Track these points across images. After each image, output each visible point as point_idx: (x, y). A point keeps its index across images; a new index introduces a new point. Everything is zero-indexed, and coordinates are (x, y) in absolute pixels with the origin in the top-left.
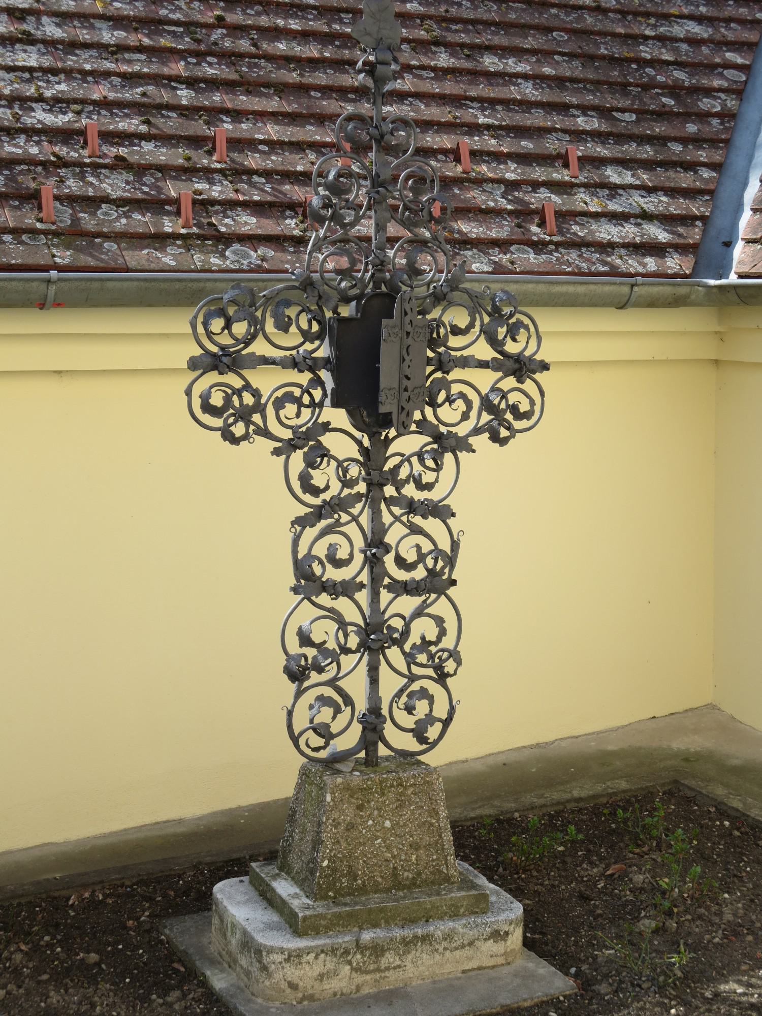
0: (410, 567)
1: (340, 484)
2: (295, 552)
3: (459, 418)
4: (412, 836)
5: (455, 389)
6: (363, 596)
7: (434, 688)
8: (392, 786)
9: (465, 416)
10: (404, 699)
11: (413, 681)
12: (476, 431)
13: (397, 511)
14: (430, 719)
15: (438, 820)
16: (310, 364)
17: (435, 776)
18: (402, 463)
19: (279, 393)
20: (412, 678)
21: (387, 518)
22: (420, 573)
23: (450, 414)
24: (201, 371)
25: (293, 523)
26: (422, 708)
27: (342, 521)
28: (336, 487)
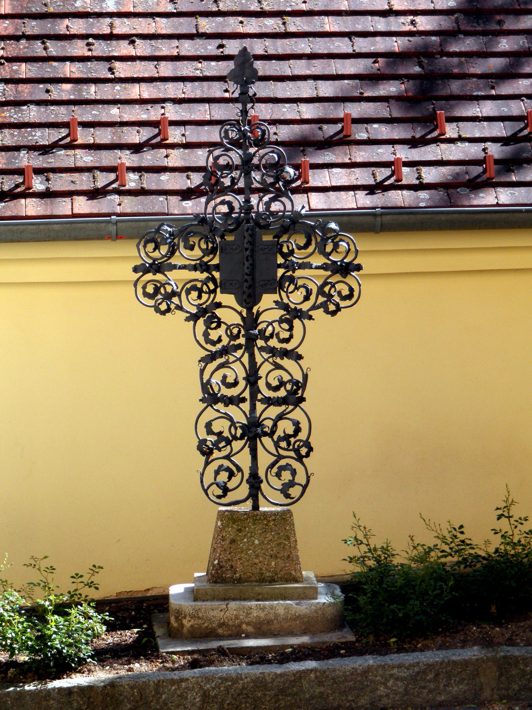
0: (276, 389)
1: (228, 339)
2: (202, 379)
3: (302, 299)
4: (272, 550)
5: (300, 282)
6: (246, 406)
7: (296, 465)
8: (260, 519)
9: (307, 298)
10: (275, 470)
11: (281, 459)
12: (314, 307)
13: (266, 356)
14: (292, 484)
15: (290, 543)
16: (203, 267)
17: (288, 515)
18: (268, 326)
19: (188, 286)
20: (280, 457)
21: (259, 359)
22: (282, 393)
23: (297, 297)
24: (141, 274)
25: (200, 361)
26: (286, 476)
27: (231, 361)
28: (225, 340)
